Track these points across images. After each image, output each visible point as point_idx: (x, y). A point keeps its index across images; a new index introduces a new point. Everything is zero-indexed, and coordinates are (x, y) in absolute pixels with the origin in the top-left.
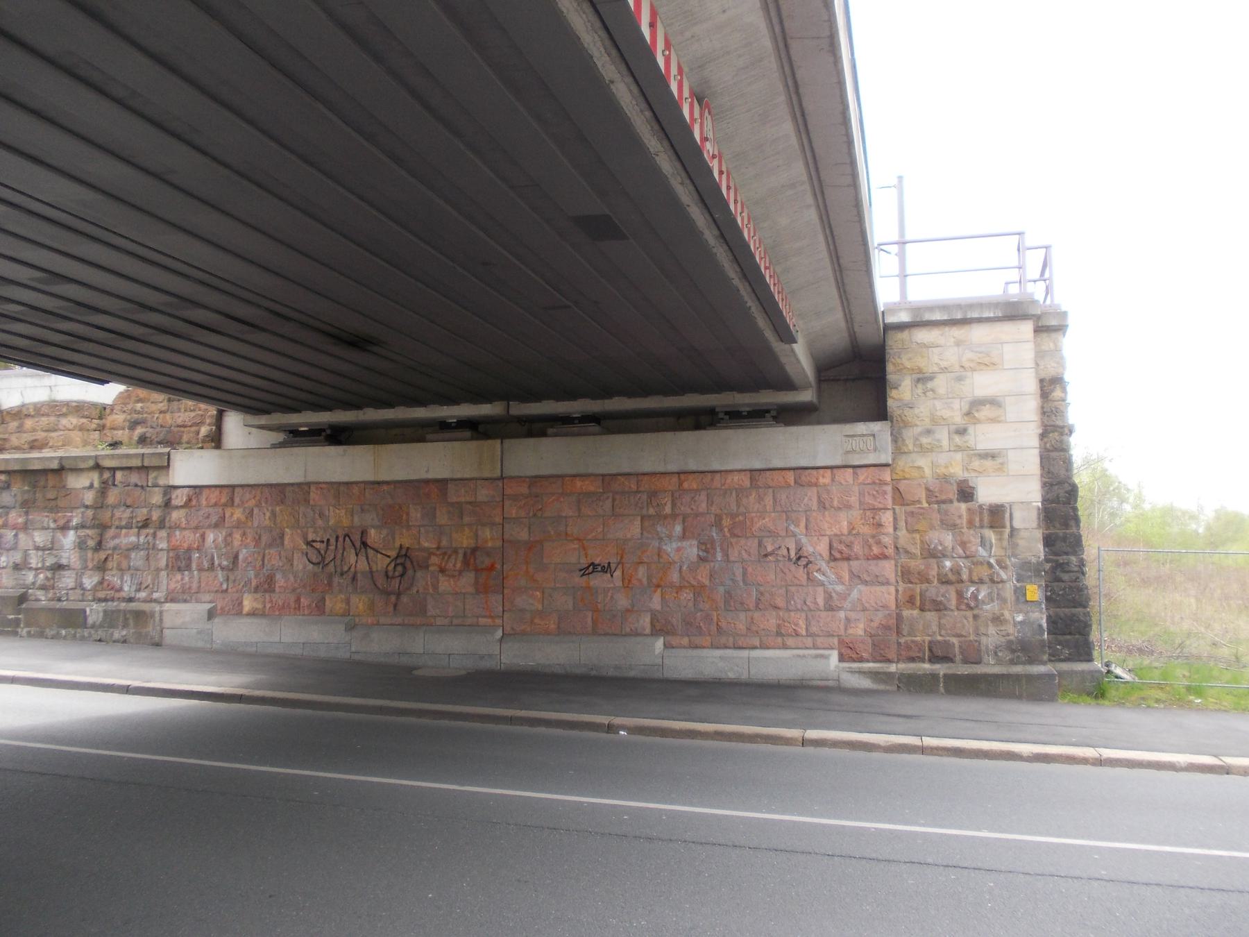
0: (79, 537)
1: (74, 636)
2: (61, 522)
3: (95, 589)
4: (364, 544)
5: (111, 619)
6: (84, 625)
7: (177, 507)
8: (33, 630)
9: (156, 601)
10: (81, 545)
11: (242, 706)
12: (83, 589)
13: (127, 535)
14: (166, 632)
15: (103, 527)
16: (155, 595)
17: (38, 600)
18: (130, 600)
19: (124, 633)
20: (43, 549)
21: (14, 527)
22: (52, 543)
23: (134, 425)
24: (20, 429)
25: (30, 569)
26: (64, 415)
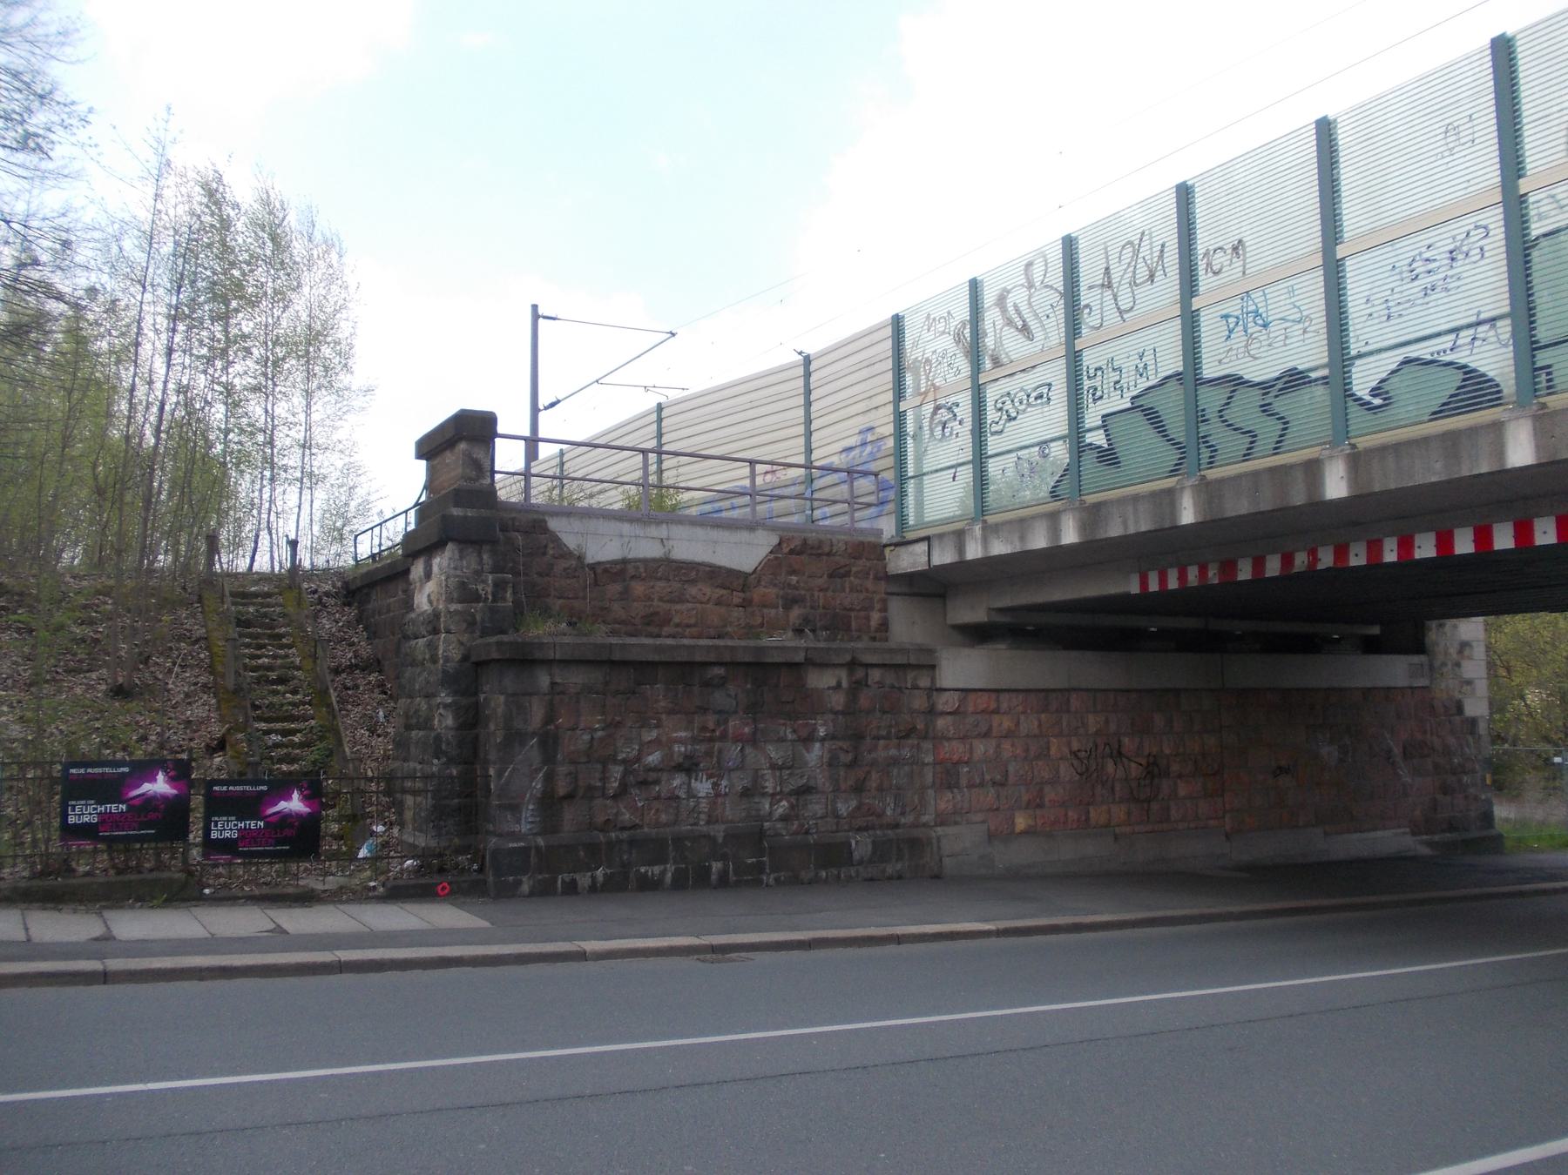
0: (830, 751)
1: (839, 877)
2: (804, 733)
3: (851, 815)
4: (1120, 753)
5: (881, 852)
6: (849, 861)
7: (943, 713)
8: (783, 875)
9: (925, 825)
10: (832, 763)
11: (1206, 926)
12: (838, 817)
13: (886, 747)
14: (946, 861)
15: (858, 737)
16: (925, 819)
17: (778, 835)
18: (897, 826)
19: (899, 866)
20: (781, 768)
21: (738, 739)
22: (794, 759)
23: (790, 603)
24: (625, 594)
25: (764, 795)
26: (693, 582)
